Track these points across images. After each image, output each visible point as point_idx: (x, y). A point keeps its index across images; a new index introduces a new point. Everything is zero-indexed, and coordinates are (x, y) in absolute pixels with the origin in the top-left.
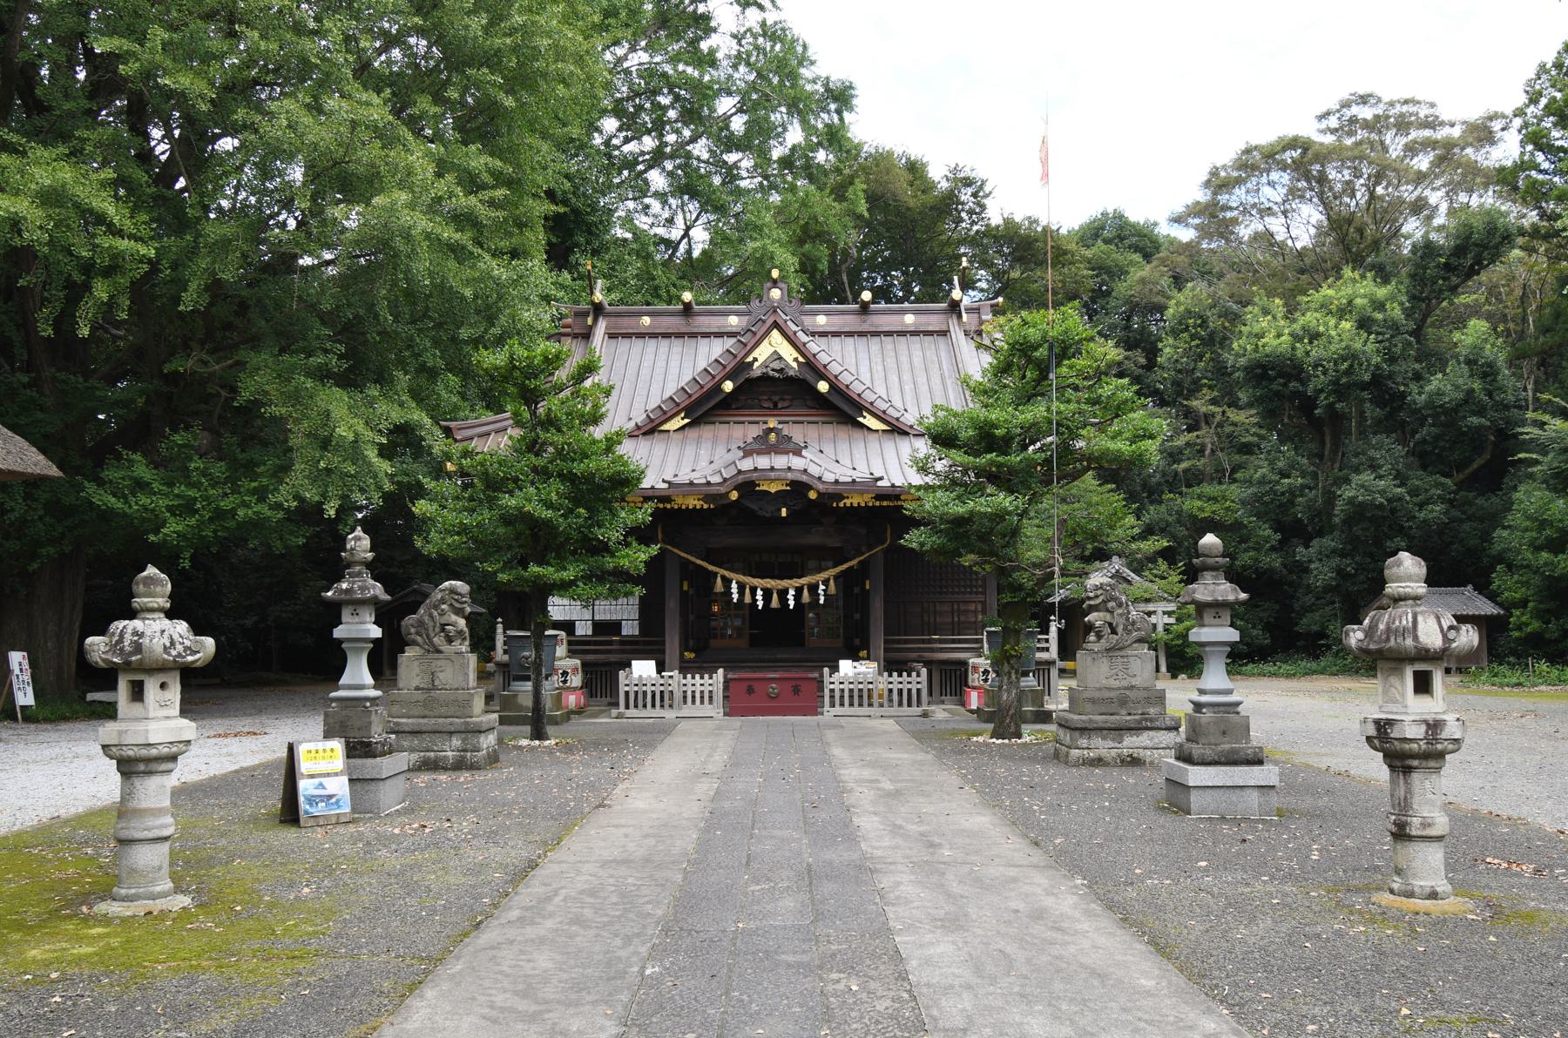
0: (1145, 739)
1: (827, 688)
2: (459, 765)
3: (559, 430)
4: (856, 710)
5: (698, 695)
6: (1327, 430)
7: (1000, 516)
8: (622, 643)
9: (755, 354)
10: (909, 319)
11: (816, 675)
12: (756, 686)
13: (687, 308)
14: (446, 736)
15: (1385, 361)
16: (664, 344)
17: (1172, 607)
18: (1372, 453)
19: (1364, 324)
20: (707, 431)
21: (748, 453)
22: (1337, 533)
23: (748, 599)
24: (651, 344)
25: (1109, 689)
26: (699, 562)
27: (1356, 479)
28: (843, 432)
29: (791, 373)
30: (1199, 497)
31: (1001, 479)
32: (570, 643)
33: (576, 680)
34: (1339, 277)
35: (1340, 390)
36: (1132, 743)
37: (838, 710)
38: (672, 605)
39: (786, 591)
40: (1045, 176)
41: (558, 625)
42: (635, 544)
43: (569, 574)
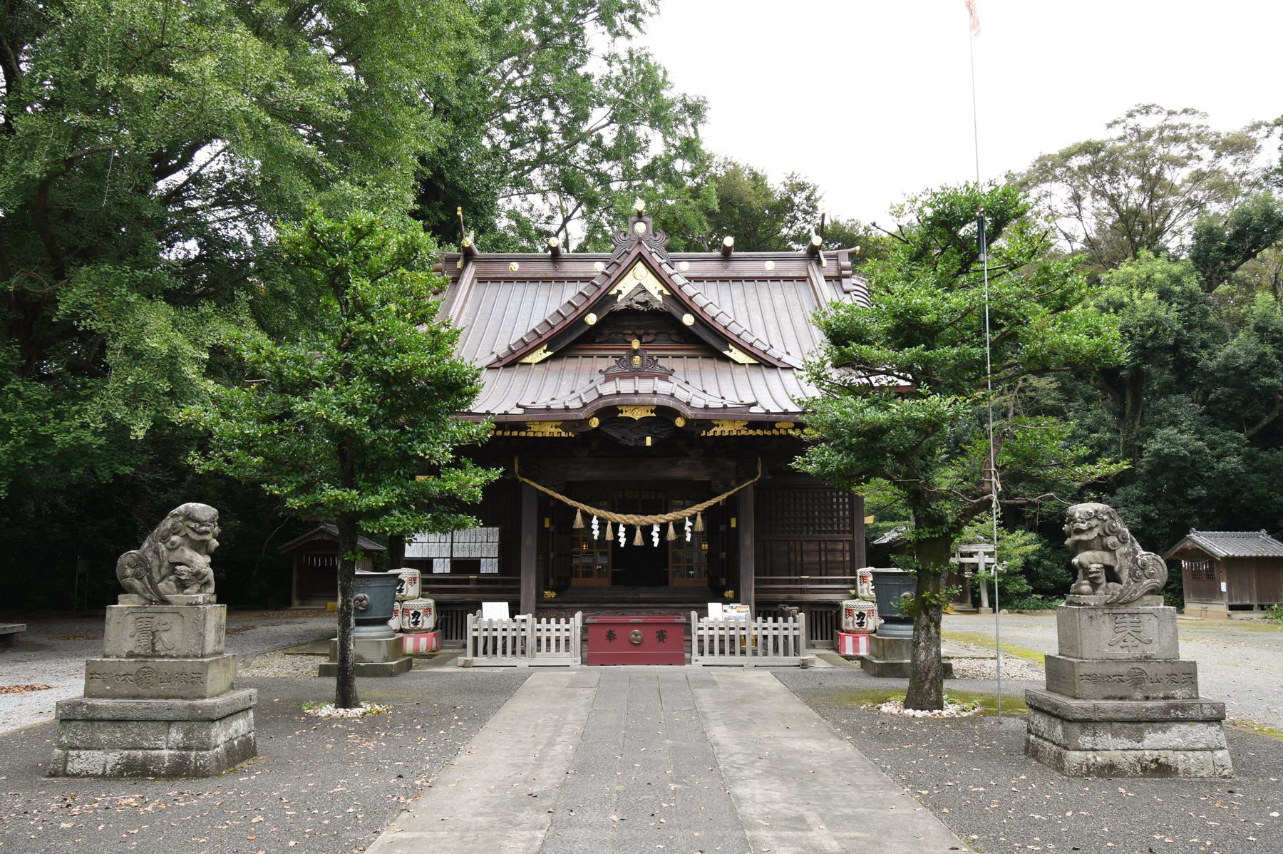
0: (1174, 735)
1: (696, 634)
2: (179, 771)
3: (368, 318)
4: (727, 659)
5: (553, 642)
6: (1128, 392)
8: (478, 581)
9: (619, 287)
10: (770, 266)
11: (683, 620)
12: (616, 630)
14: (161, 727)
15: (1184, 327)
16: (532, 287)
17: (991, 549)
18: (1172, 410)
19: (1165, 295)
20: (570, 364)
22: (1139, 483)
23: (609, 536)
24: (519, 287)
25: (1118, 661)
26: (558, 496)
28: (709, 365)
29: (656, 306)
31: (926, 377)
32: (424, 581)
33: (428, 622)
34: (1136, 257)
36: (1156, 742)
37: (707, 658)
38: (529, 542)
39: (650, 528)
40: (975, 25)
41: (412, 563)
42: (469, 465)
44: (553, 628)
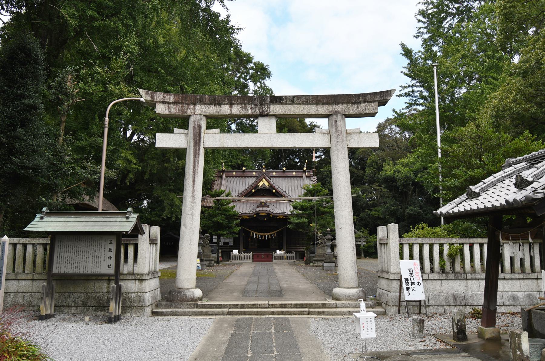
4: (280, 261)
7: (304, 223)
13: (244, 171)
17: (365, 240)
21: (258, 207)
27: (410, 208)
30: (375, 211)
35: (405, 185)
37: (276, 261)
43: (225, 233)
44: (247, 255)
